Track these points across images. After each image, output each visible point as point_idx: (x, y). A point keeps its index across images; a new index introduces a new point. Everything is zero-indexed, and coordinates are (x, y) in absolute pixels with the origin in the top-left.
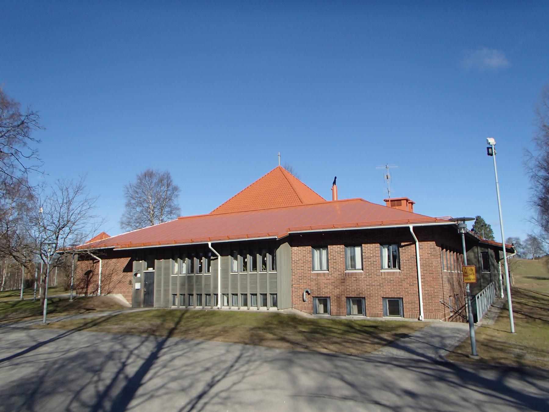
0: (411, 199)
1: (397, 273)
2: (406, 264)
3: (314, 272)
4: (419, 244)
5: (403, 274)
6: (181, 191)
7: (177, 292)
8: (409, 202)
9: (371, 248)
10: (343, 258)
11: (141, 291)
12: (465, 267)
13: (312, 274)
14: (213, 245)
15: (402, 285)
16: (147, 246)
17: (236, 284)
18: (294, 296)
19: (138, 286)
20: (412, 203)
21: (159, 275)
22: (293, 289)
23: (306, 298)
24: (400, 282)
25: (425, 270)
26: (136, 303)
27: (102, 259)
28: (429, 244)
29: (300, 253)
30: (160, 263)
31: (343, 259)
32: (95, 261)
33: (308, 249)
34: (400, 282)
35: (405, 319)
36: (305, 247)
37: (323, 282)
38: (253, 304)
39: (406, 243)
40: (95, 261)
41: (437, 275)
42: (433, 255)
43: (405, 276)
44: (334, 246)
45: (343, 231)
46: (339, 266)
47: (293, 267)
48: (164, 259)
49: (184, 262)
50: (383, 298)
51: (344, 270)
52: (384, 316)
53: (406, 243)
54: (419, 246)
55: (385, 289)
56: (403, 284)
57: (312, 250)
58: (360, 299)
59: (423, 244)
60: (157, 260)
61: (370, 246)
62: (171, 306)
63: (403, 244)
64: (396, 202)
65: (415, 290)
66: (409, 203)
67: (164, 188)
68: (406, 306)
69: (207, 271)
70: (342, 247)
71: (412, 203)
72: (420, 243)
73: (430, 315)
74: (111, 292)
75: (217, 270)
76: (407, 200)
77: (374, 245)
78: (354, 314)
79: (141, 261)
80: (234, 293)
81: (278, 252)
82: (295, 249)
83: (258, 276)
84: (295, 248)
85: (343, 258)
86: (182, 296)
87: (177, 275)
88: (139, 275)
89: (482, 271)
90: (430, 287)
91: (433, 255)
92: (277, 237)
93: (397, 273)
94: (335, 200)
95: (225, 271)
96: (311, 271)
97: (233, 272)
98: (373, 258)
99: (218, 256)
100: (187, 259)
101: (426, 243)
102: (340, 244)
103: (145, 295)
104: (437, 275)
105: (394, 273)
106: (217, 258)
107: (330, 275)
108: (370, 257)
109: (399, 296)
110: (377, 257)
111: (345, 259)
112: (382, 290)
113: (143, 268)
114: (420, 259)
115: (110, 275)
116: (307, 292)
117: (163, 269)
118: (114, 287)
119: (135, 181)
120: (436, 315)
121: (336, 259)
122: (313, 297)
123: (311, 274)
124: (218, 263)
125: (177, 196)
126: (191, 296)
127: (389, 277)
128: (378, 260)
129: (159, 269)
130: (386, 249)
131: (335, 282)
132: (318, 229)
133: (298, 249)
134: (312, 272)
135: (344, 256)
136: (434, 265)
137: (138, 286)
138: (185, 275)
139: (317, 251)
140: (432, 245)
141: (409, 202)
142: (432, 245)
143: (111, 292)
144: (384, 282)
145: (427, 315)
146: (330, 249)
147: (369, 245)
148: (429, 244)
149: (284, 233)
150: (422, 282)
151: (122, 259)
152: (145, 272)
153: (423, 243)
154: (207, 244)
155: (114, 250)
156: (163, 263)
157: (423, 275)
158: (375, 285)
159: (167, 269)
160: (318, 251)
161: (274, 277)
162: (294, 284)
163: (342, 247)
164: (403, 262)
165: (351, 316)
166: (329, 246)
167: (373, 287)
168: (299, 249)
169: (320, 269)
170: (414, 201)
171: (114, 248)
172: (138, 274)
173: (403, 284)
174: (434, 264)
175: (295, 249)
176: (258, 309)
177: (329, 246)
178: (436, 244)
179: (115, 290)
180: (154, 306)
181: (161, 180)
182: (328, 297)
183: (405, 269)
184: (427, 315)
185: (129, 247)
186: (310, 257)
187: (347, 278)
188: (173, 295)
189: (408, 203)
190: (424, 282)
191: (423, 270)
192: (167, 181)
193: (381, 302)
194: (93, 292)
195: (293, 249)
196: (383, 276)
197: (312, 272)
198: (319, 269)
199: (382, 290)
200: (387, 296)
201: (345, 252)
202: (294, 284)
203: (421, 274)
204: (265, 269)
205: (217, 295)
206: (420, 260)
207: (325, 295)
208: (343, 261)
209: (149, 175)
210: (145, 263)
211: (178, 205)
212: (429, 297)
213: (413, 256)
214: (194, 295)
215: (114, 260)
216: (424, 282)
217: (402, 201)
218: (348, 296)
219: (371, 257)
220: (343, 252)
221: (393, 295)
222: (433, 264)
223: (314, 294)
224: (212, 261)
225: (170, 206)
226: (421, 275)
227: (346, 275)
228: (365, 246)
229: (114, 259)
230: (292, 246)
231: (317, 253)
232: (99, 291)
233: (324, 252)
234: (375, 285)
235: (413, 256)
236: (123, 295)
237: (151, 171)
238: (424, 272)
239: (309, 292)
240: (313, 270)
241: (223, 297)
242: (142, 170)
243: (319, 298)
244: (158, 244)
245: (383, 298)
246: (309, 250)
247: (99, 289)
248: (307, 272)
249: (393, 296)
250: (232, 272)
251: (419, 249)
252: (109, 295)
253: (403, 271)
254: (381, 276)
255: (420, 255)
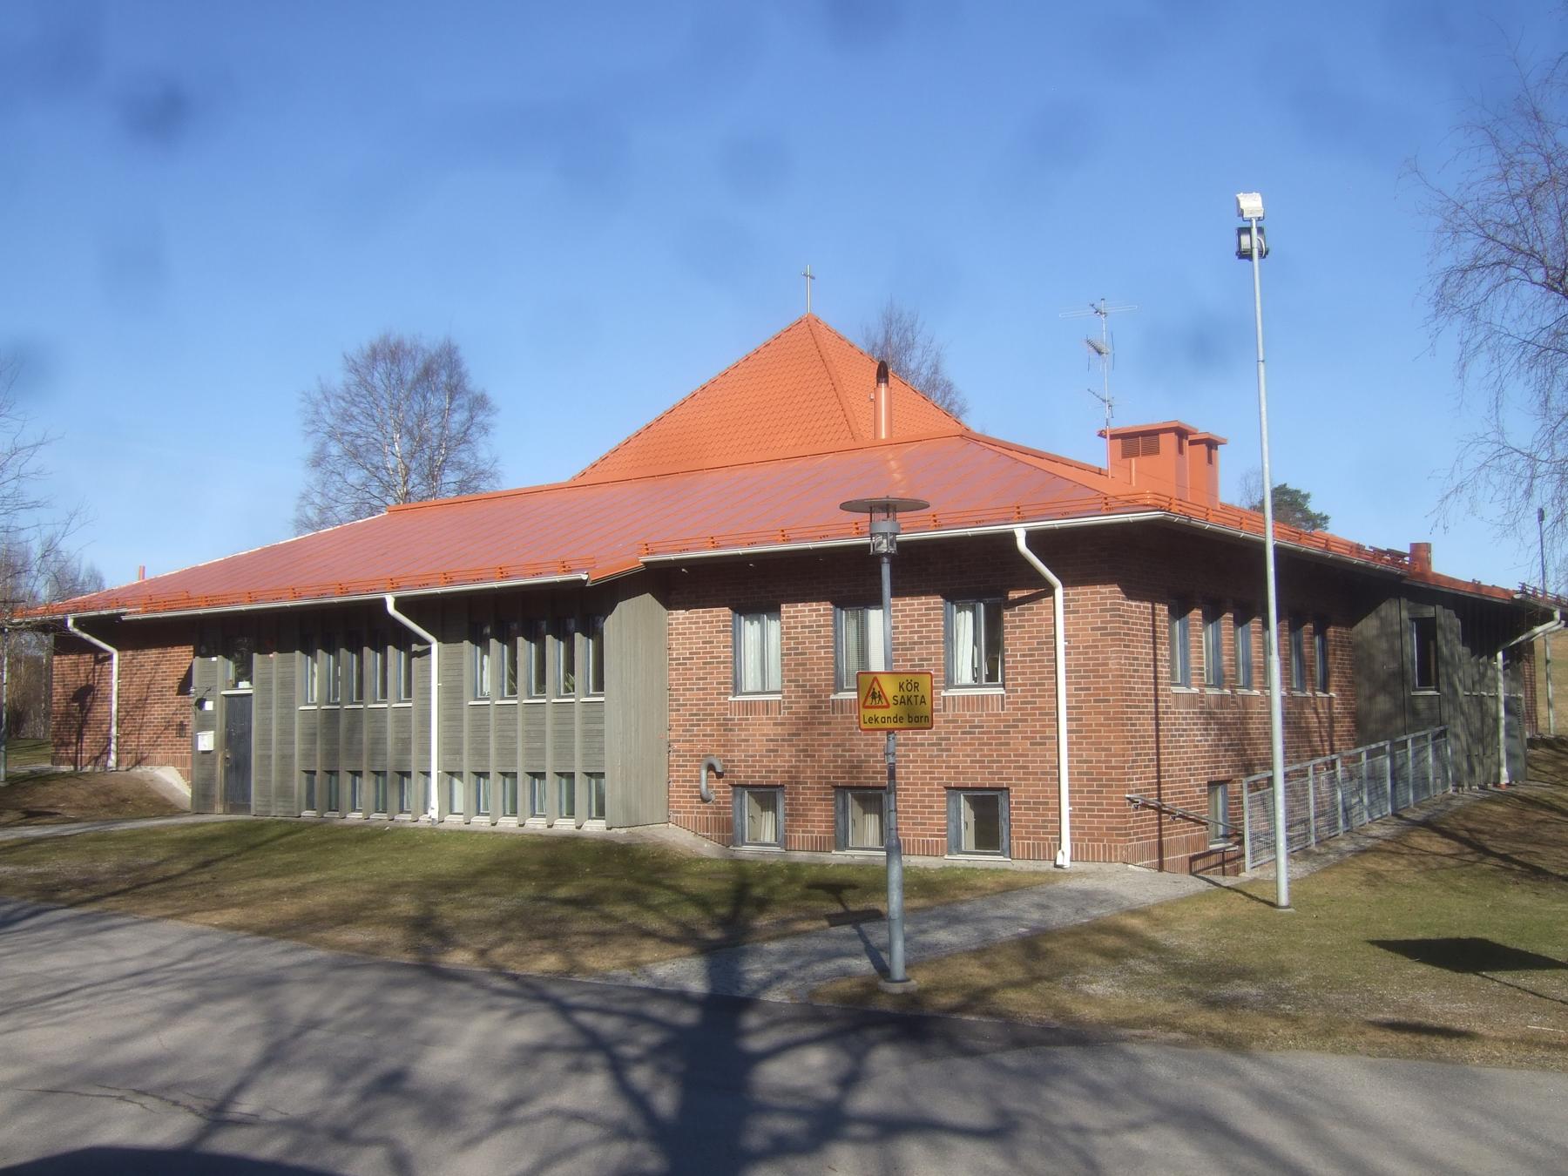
0: (1202, 425)
1: (993, 700)
2: (1023, 667)
3: (739, 698)
4: (1065, 595)
5: (1012, 703)
6: (498, 410)
7: (514, 763)
8: (1191, 438)
9: (915, 610)
10: (828, 647)
11: (215, 758)
12: (872, 676)
13: (944, 701)
14: (401, 604)
15: (1008, 744)
16: (214, 606)
17: (485, 741)
18: (674, 781)
19: (206, 741)
20: (1211, 444)
21: (266, 705)
22: (671, 758)
23: (710, 790)
24: (1001, 732)
25: (1081, 689)
26: (203, 797)
27: (119, 650)
28: (1100, 593)
29: (694, 633)
30: (267, 664)
31: (825, 653)
32: (100, 656)
33: (719, 616)
34: (1001, 732)
35: (1014, 862)
36: (709, 612)
37: (764, 735)
38: (537, 808)
39: (1025, 593)
40: (100, 656)
41: (1122, 706)
42: (1109, 634)
43: (1020, 709)
44: (800, 606)
45: (808, 550)
46: (815, 675)
47: (674, 680)
48: (280, 652)
49: (315, 660)
50: (947, 788)
51: (828, 691)
52: (950, 853)
53: (1025, 593)
54: (1065, 601)
55: (954, 756)
56: (1011, 738)
57: (734, 621)
58: (879, 792)
59: (1078, 594)
60: (260, 653)
61: (913, 604)
62: (300, 812)
63: (1014, 595)
64: (1136, 442)
65: (1048, 762)
66: (1192, 443)
67: (437, 401)
68: (1017, 817)
69: (402, 695)
70: (824, 610)
71: (1211, 444)
72: (1071, 591)
73: (1093, 846)
74: (146, 758)
75: (428, 690)
76: (1181, 433)
77: (923, 599)
78: (870, 845)
79: (214, 659)
80: (480, 770)
81: (611, 625)
82: (681, 617)
83: (520, 710)
84: (681, 614)
85: (828, 647)
86: (507, 780)
87: (338, 707)
88: (209, 706)
89: (1415, 690)
90: (1096, 750)
91: (1109, 634)
92: (585, 577)
93: (993, 700)
94: (883, 436)
95: (452, 694)
96: (828, 691)
97: (479, 696)
98: (919, 649)
99: (429, 643)
100: (319, 651)
101: (1088, 589)
102: (818, 600)
103: (228, 771)
104: (1122, 706)
105: (983, 699)
106: (428, 652)
107: (785, 708)
108: (910, 643)
109: (997, 783)
110: (933, 643)
111: (836, 652)
112: (944, 762)
113: (220, 682)
114: (1066, 648)
115: (142, 703)
116: (711, 767)
117: (274, 687)
118: (154, 745)
119: (339, 378)
120: (1110, 846)
121: (805, 654)
122: (733, 785)
123: (726, 704)
124: (430, 665)
125: (485, 429)
126: (539, 779)
127: (765, 716)
128: (935, 654)
129: (265, 685)
130: (969, 615)
131: (800, 735)
132: (839, 535)
133: (688, 618)
134: (730, 698)
135: (828, 642)
136: (1111, 670)
137: (206, 741)
138: (778, 697)
139: (752, 624)
140: (1106, 598)
141: (1191, 438)
142: (1106, 598)
143: (146, 758)
144: (951, 733)
145: (1082, 849)
146: (787, 617)
147: (908, 600)
148: (1100, 593)
149: (627, 558)
150: (1069, 732)
151: (176, 649)
152: (225, 696)
153: (1080, 589)
154: (383, 602)
155: (124, 618)
156: (275, 663)
157: (1074, 708)
158: (923, 745)
159: (287, 685)
160: (756, 622)
161: (595, 713)
162: (674, 741)
163: (825, 607)
164: (1013, 662)
165: (847, 852)
166: (784, 607)
167: (916, 750)
168: (692, 618)
169: (975, 679)
170: (1216, 432)
171: (124, 614)
172: (205, 700)
173: (1011, 738)
174: (1112, 664)
175: (681, 617)
176: (520, 826)
177: (784, 607)
178: (1124, 592)
179: (158, 754)
180: (253, 812)
181: (427, 373)
182: (777, 786)
183: (1020, 685)
184: (1082, 849)
185: (165, 611)
186: (724, 647)
187: (837, 718)
188: (305, 775)
189: (1186, 443)
190: (1077, 732)
191: (1076, 689)
192: (450, 377)
193: (940, 803)
194: (97, 759)
195: (673, 619)
196: (950, 712)
197: (730, 698)
198: (759, 689)
199: (944, 762)
200: (961, 782)
201: (835, 625)
202: (674, 741)
203: (1068, 702)
204: (569, 689)
205: (427, 774)
206: (1067, 654)
207: (770, 777)
208: (827, 658)
209: (390, 353)
210: (228, 667)
211: (496, 461)
212: (1089, 782)
213: (1046, 637)
214: (492, 776)
215: (153, 654)
216: (1077, 732)
217: (1161, 436)
218: (840, 782)
219: (915, 643)
220: (827, 626)
221: (981, 778)
222: (1110, 666)
223: (734, 777)
224: (414, 660)
225: (460, 466)
226: (1068, 708)
227: (833, 709)
228: (913, 604)
229: (154, 651)
230: (670, 604)
231: (751, 630)
232: (113, 757)
233: (774, 627)
234: (923, 745)
235: (1046, 637)
236: (180, 771)
237: (393, 340)
238: (1080, 695)
239: (719, 770)
240: (737, 688)
241: (451, 783)
242: (362, 335)
243: (751, 790)
244: (247, 599)
245: (947, 788)
246: (723, 621)
247: (113, 747)
248: (716, 699)
249: (979, 782)
250: (476, 699)
251: (1065, 613)
252: (139, 770)
253: (1012, 691)
254: (945, 711)
255: (1066, 636)
